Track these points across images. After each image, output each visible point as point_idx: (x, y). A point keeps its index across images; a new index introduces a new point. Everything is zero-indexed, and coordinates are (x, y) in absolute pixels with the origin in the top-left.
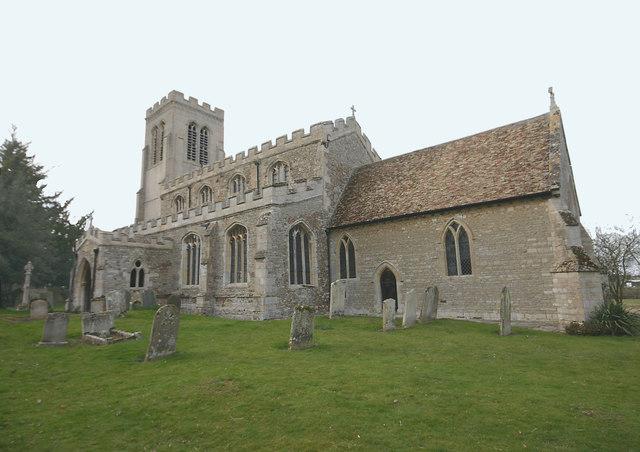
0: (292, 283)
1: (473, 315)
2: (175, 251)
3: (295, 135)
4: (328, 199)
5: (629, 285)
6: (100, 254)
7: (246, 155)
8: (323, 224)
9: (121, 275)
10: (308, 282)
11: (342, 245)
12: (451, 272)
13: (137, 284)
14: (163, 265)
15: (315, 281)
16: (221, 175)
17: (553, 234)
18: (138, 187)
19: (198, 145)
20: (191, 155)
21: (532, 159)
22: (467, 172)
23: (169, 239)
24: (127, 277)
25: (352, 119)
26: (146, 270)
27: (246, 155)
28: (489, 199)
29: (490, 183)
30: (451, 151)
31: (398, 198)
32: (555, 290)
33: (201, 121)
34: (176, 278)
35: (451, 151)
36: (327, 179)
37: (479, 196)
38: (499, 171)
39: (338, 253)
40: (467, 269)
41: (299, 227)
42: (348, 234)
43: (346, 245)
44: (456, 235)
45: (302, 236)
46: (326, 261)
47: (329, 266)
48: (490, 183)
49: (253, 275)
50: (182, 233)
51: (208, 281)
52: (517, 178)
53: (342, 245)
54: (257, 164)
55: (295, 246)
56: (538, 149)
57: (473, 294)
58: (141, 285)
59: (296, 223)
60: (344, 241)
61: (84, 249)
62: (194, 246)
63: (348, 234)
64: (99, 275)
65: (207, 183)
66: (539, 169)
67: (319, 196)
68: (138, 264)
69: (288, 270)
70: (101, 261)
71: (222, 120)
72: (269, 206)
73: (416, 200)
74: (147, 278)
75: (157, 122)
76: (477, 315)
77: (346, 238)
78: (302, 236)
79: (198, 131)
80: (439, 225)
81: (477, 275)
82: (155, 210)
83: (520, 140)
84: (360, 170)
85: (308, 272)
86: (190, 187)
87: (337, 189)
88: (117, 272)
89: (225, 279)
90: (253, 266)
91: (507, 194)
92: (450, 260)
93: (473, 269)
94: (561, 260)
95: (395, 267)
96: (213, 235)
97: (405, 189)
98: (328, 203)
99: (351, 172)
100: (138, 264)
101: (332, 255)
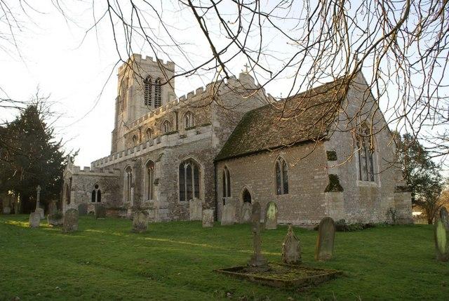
2: (120, 178)
4: (217, 139)
5: (62, 163)
6: (73, 181)
7: (195, 93)
8: (211, 157)
9: (86, 194)
12: (279, 193)
13: (96, 200)
18: (113, 128)
20: (148, 102)
23: (118, 169)
24: (90, 195)
27: (195, 93)
34: (121, 196)
36: (216, 124)
42: (226, 165)
45: (193, 168)
47: (216, 188)
51: (135, 199)
53: (224, 172)
61: (66, 176)
63: (226, 165)
64: (73, 193)
67: (211, 138)
70: (73, 185)
72: (164, 148)
77: (226, 168)
78: (193, 168)
81: (291, 194)
82: (122, 144)
88: (83, 192)
89: (145, 198)
92: (278, 184)
95: (249, 187)
100: (97, 187)
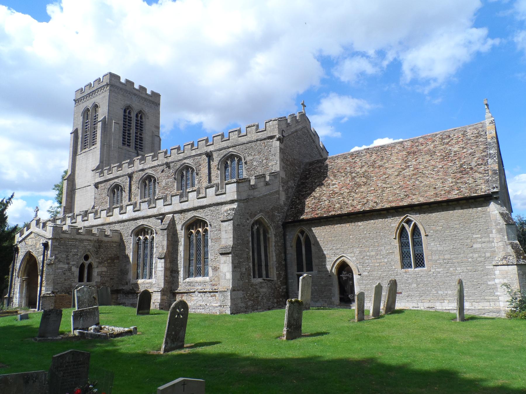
0: (254, 277)
1: (427, 305)
3: (249, 129)
8: (279, 217)
9: (70, 269)
10: (267, 276)
11: (299, 239)
12: (405, 265)
14: (111, 258)
15: (274, 274)
16: (168, 165)
17: (494, 231)
19: (133, 131)
21: (473, 164)
22: (417, 173)
24: (76, 271)
25: (303, 116)
26: (95, 264)
28: (439, 199)
29: (439, 184)
30: (400, 151)
31: (353, 194)
32: (497, 281)
33: (136, 106)
35: (400, 151)
37: (429, 197)
38: (446, 173)
39: (295, 246)
40: (420, 262)
41: (258, 222)
43: (302, 239)
44: (409, 230)
46: (283, 255)
48: (439, 184)
49: (215, 269)
50: (133, 225)
52: (462, 180)
53: (299, 239)
54: (209, 155)
55: (255, 240)
56: (478, 155)
57: (427, 285)
58: (89, 280)
59: (256, 218)
60: (300, 235)
62: (146, 239)
65: (150, 172)
66: (480, 173)
68: (86, 258)
69: (251, 265)
71: (158, 104)
73: (371, 197)
74: (95, 272)
75: (89, 104)
76: (430, 305)
79: (133, 115)
80: (395, 222)
83: (461, 144)
84: (311, 164)
85: (267, 265)
86: (130, 176)
87: (291, 183)
88: (66, 266)
90: (156, 263)
91: (454, 195)
93: (425, 263)
94: (501, 254)
96: (171, 230)
97: (359, 186)
98: (283, 197)
99: (302, 166)
101: (289, 248)
